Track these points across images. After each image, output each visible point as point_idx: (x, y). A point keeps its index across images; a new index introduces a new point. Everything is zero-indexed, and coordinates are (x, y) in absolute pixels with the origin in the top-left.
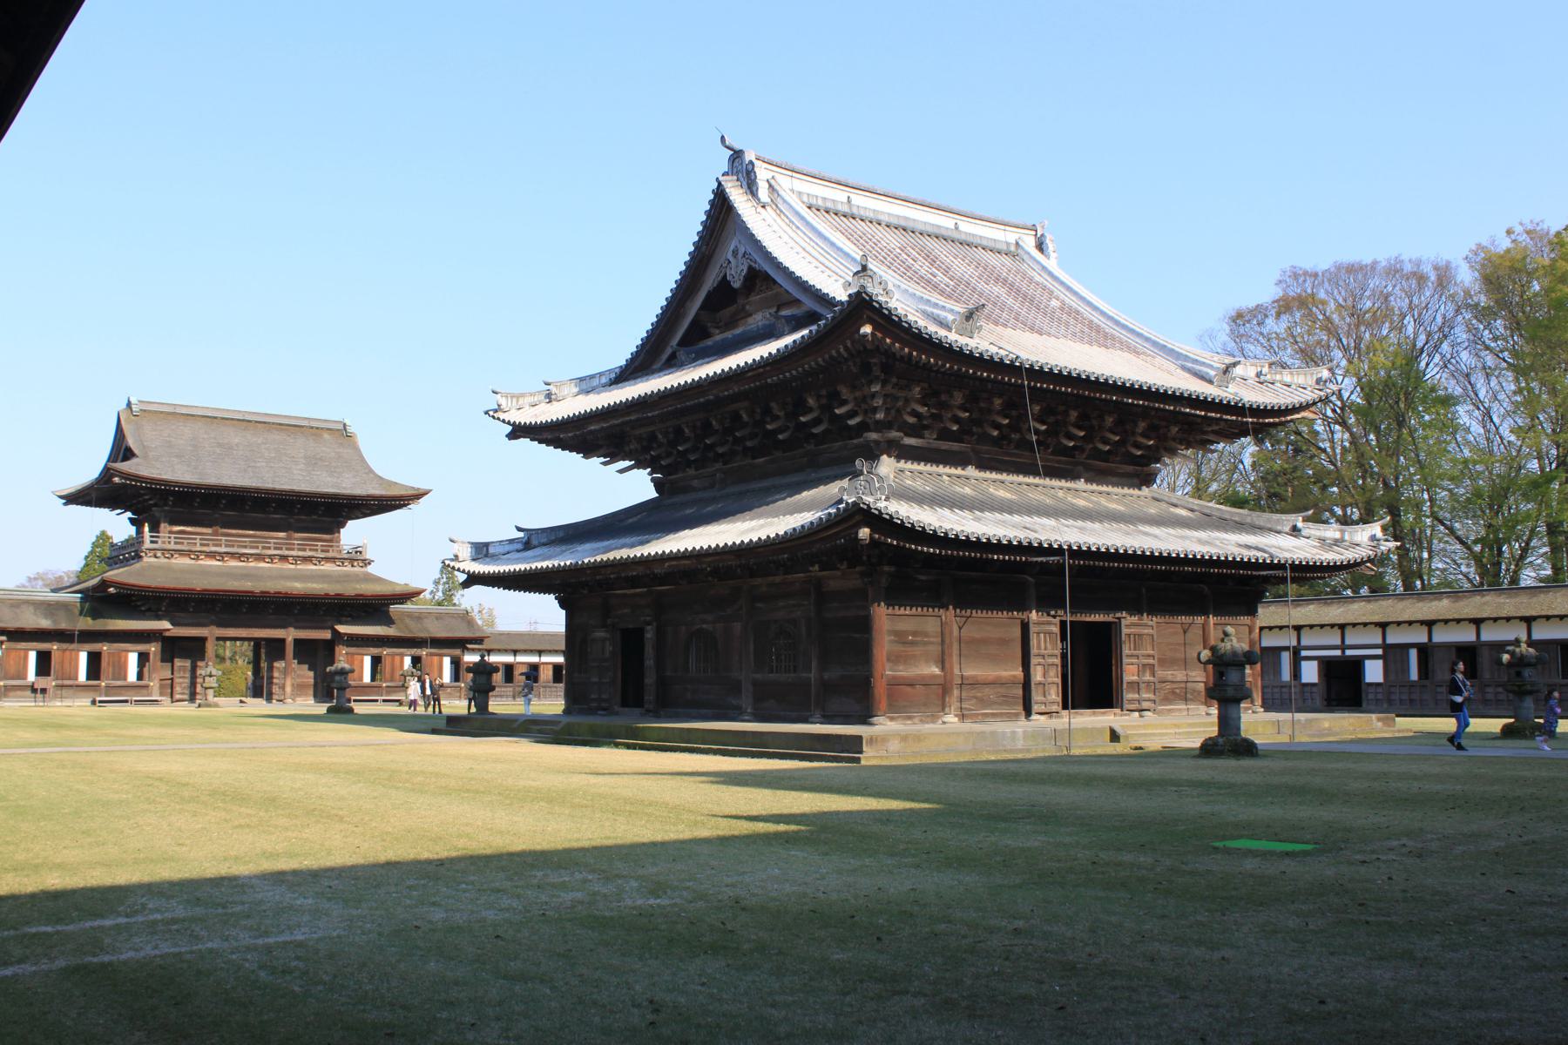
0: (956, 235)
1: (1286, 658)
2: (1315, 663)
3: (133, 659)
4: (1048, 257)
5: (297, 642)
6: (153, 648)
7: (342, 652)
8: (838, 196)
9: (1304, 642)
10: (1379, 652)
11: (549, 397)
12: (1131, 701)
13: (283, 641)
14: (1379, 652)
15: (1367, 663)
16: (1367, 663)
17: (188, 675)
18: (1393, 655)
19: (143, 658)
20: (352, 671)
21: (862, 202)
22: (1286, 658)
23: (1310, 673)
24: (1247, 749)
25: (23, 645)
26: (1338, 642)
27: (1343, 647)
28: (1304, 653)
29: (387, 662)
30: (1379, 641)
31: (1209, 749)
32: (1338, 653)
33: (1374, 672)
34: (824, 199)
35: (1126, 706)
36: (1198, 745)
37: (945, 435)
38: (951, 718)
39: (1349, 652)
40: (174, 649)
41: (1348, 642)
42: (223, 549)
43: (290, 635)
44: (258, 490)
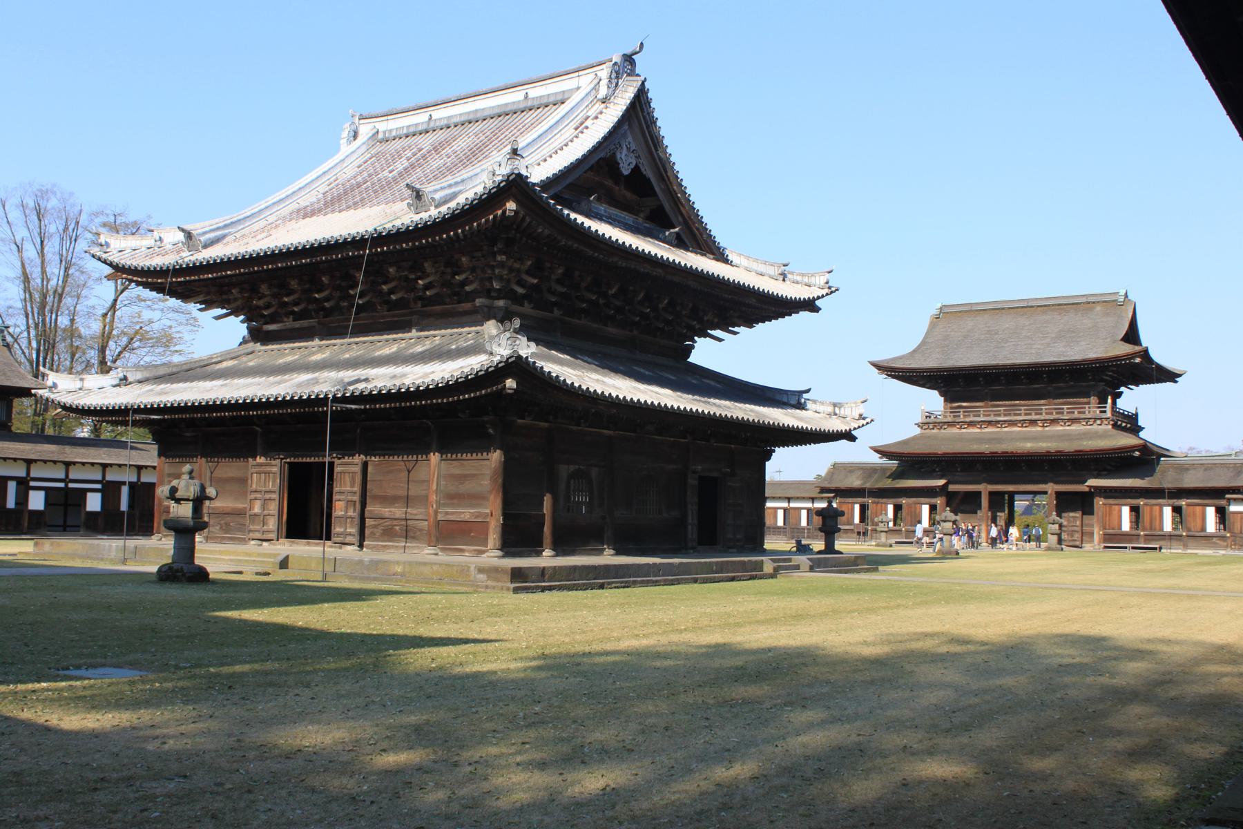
0: (529, 104)
1: (12, 487)
2: (42, 494)
3: (925, 509)
4: (349, 142)
5: (991, 494)
6: (939, 501)
7: (1099, 502)
8: (421, 118)
9: (33, 475)
10: (99, 486)
11: (784, 276)
12: (339, 534)
13: (979, 494)
14: (99, 486)
15: (89, 495)
16: (89, 495)
17: (367, 514)
18: (110, 490)
19: (933, 508)
20: (842, 514)
21: (441, 114)
22: (12, 487)
23: (37, 501)
24: (201, 576)
25: (850, 500)
26: (62, 476)
27: (66, 480)
28: (32, 484)
29: (1146, 514)
30: (99, 478)
31: (168, 575)
32: (62, 485)
33: (94, 503)
34: (408, 127)
35: (334, 539)
36: (154, 569)
37: (298, 317)
38: (547, 552)
39: (71, 485)
40: (1065, 503)
41: (71, 476)
42: (982, 418)
43: (984, 489)
44: (985, 368)
